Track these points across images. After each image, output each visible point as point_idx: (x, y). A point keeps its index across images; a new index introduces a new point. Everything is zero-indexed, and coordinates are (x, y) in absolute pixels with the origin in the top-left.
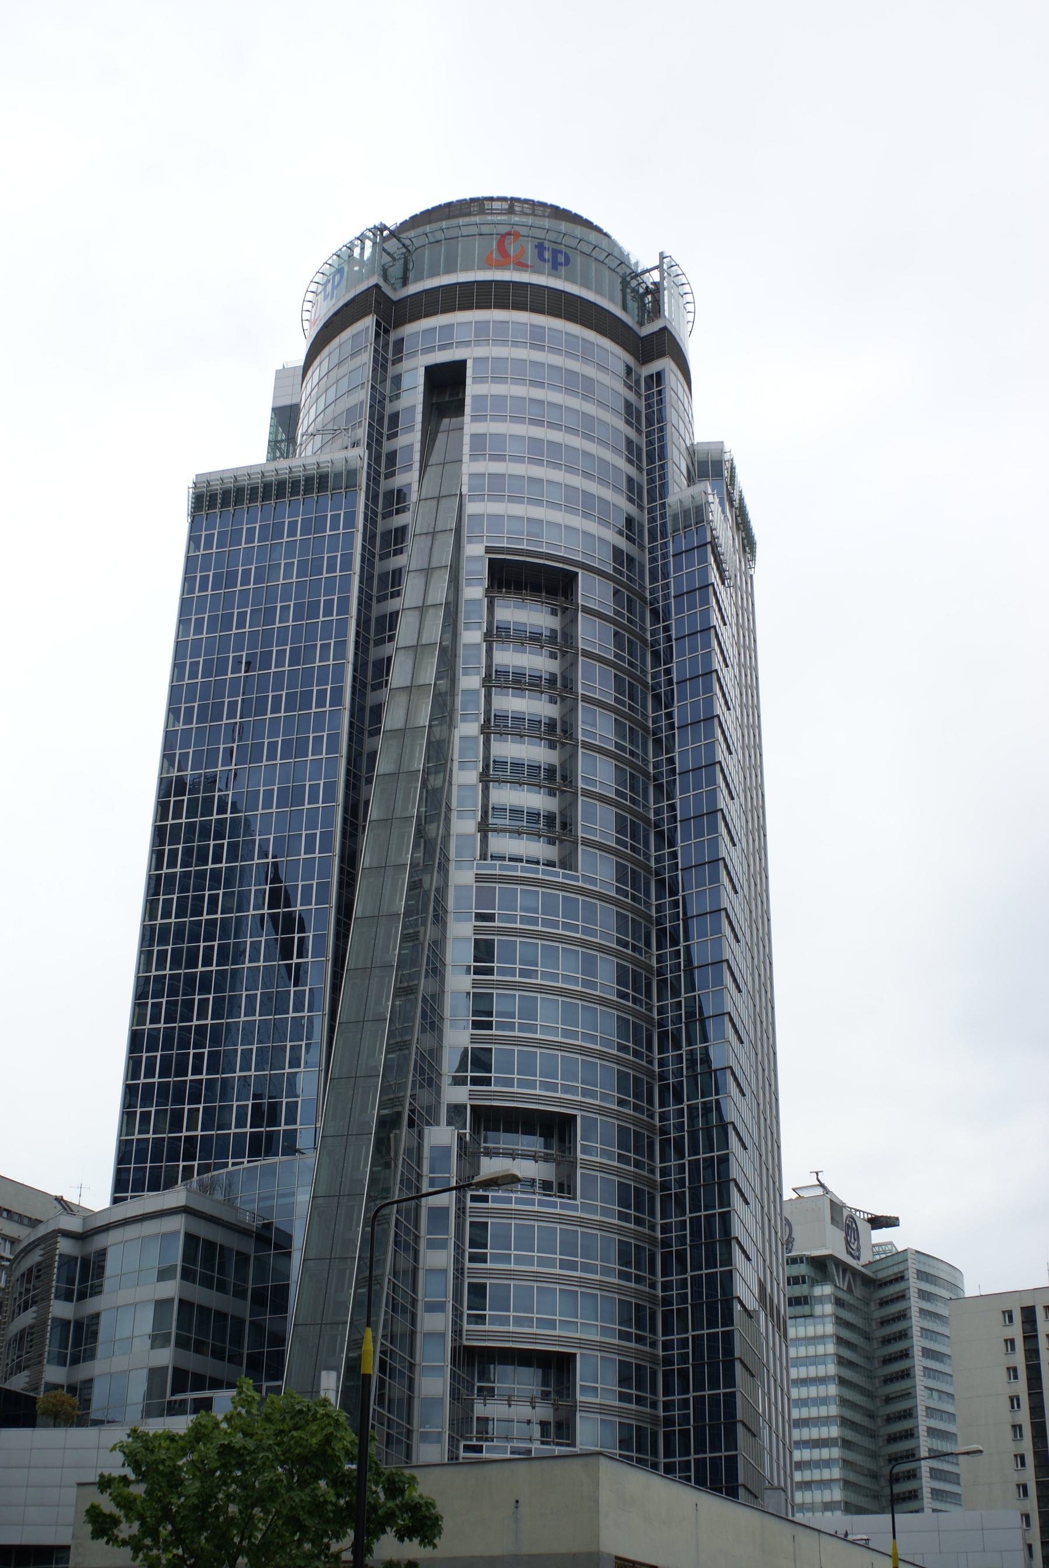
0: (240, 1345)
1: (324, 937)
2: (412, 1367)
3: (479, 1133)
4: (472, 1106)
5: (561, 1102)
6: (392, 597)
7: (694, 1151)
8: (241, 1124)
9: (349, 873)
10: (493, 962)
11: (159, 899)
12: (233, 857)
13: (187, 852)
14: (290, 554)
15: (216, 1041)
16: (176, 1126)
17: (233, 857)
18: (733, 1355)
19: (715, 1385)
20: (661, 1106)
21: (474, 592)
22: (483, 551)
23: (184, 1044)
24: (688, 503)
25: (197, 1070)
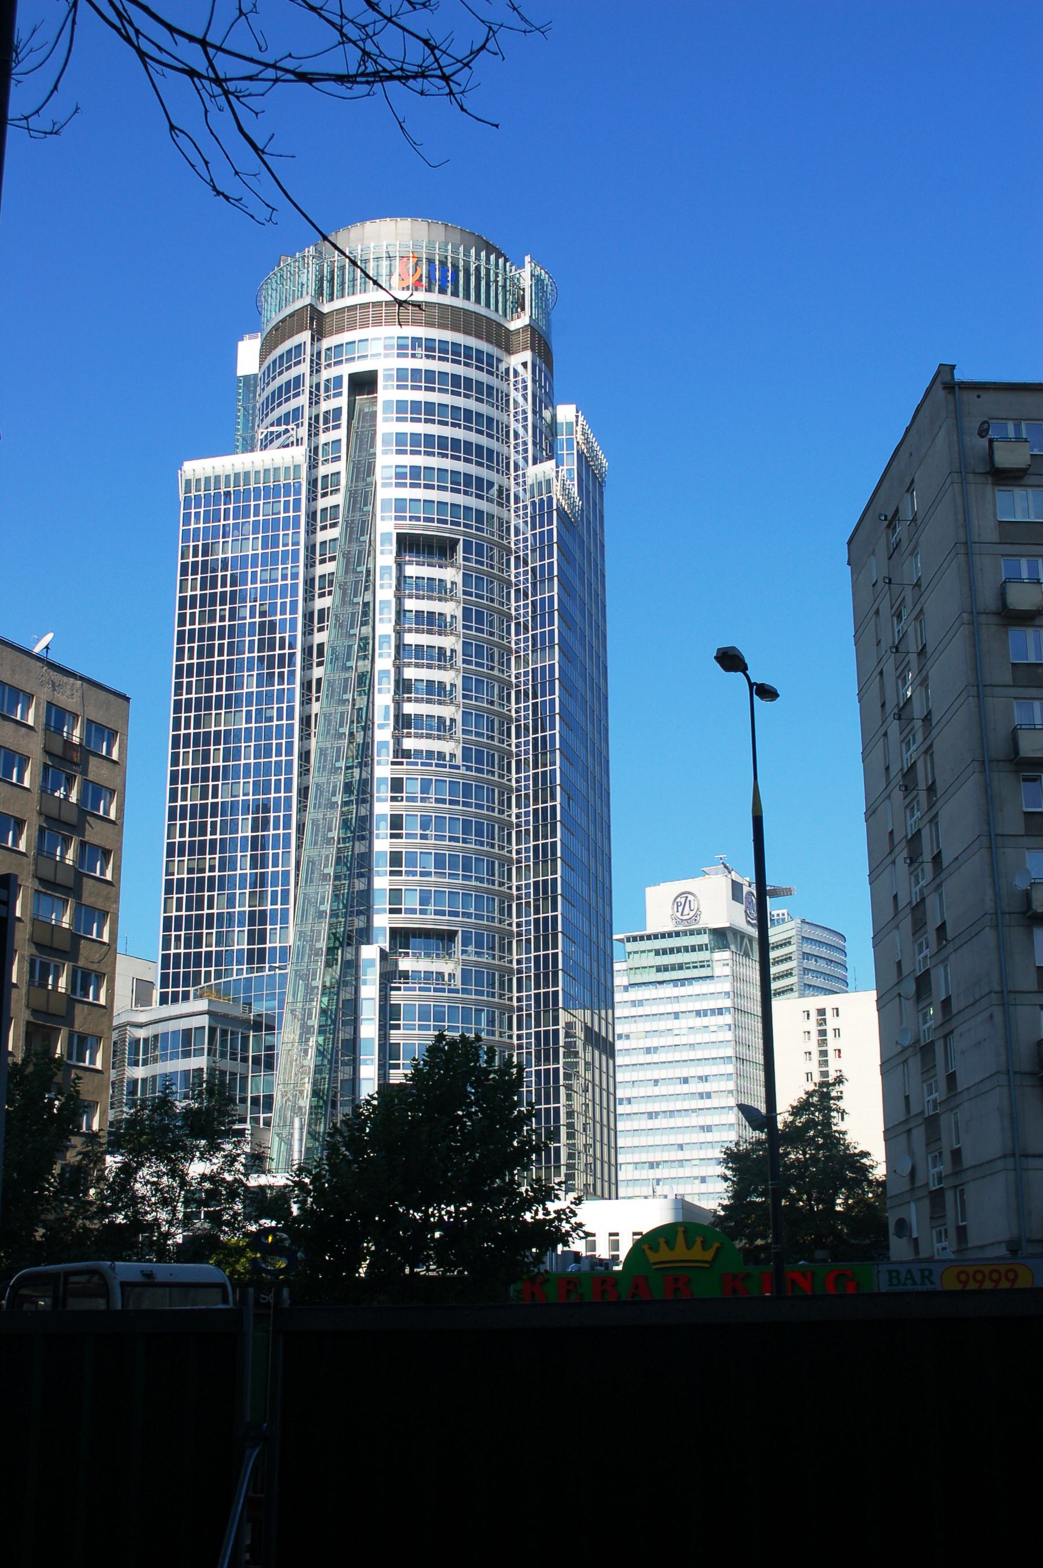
0: (247, 1051)
1: (293, 707)
2: (357, 979)
3: (396, 939)
4: (390, 928)
5: (451, 531)
6: (331, 494)
7: (535, 697)
8: (251, 651)
9: (311, 592)
10: (399, 1020)
11: (189, 546)
12: (234, 584)
13: (189, 899)
14: (256, 531)
15: (230, 670)
16: (209, 689)
17: (234, 584)
18: (560, 1162)
19: (547, 986)
20: (517, 738)
21: (385, 558)
22: (393, 527)
23: (210, 672)
24: (541, 478)
25: (213, 833)
